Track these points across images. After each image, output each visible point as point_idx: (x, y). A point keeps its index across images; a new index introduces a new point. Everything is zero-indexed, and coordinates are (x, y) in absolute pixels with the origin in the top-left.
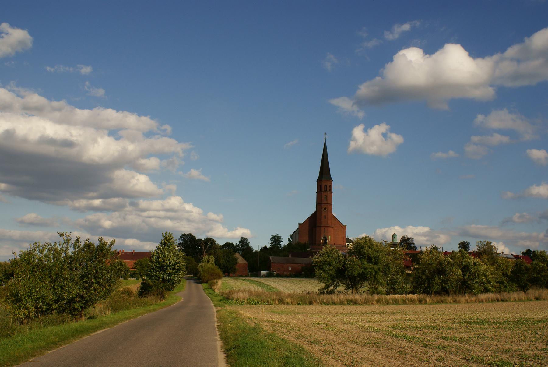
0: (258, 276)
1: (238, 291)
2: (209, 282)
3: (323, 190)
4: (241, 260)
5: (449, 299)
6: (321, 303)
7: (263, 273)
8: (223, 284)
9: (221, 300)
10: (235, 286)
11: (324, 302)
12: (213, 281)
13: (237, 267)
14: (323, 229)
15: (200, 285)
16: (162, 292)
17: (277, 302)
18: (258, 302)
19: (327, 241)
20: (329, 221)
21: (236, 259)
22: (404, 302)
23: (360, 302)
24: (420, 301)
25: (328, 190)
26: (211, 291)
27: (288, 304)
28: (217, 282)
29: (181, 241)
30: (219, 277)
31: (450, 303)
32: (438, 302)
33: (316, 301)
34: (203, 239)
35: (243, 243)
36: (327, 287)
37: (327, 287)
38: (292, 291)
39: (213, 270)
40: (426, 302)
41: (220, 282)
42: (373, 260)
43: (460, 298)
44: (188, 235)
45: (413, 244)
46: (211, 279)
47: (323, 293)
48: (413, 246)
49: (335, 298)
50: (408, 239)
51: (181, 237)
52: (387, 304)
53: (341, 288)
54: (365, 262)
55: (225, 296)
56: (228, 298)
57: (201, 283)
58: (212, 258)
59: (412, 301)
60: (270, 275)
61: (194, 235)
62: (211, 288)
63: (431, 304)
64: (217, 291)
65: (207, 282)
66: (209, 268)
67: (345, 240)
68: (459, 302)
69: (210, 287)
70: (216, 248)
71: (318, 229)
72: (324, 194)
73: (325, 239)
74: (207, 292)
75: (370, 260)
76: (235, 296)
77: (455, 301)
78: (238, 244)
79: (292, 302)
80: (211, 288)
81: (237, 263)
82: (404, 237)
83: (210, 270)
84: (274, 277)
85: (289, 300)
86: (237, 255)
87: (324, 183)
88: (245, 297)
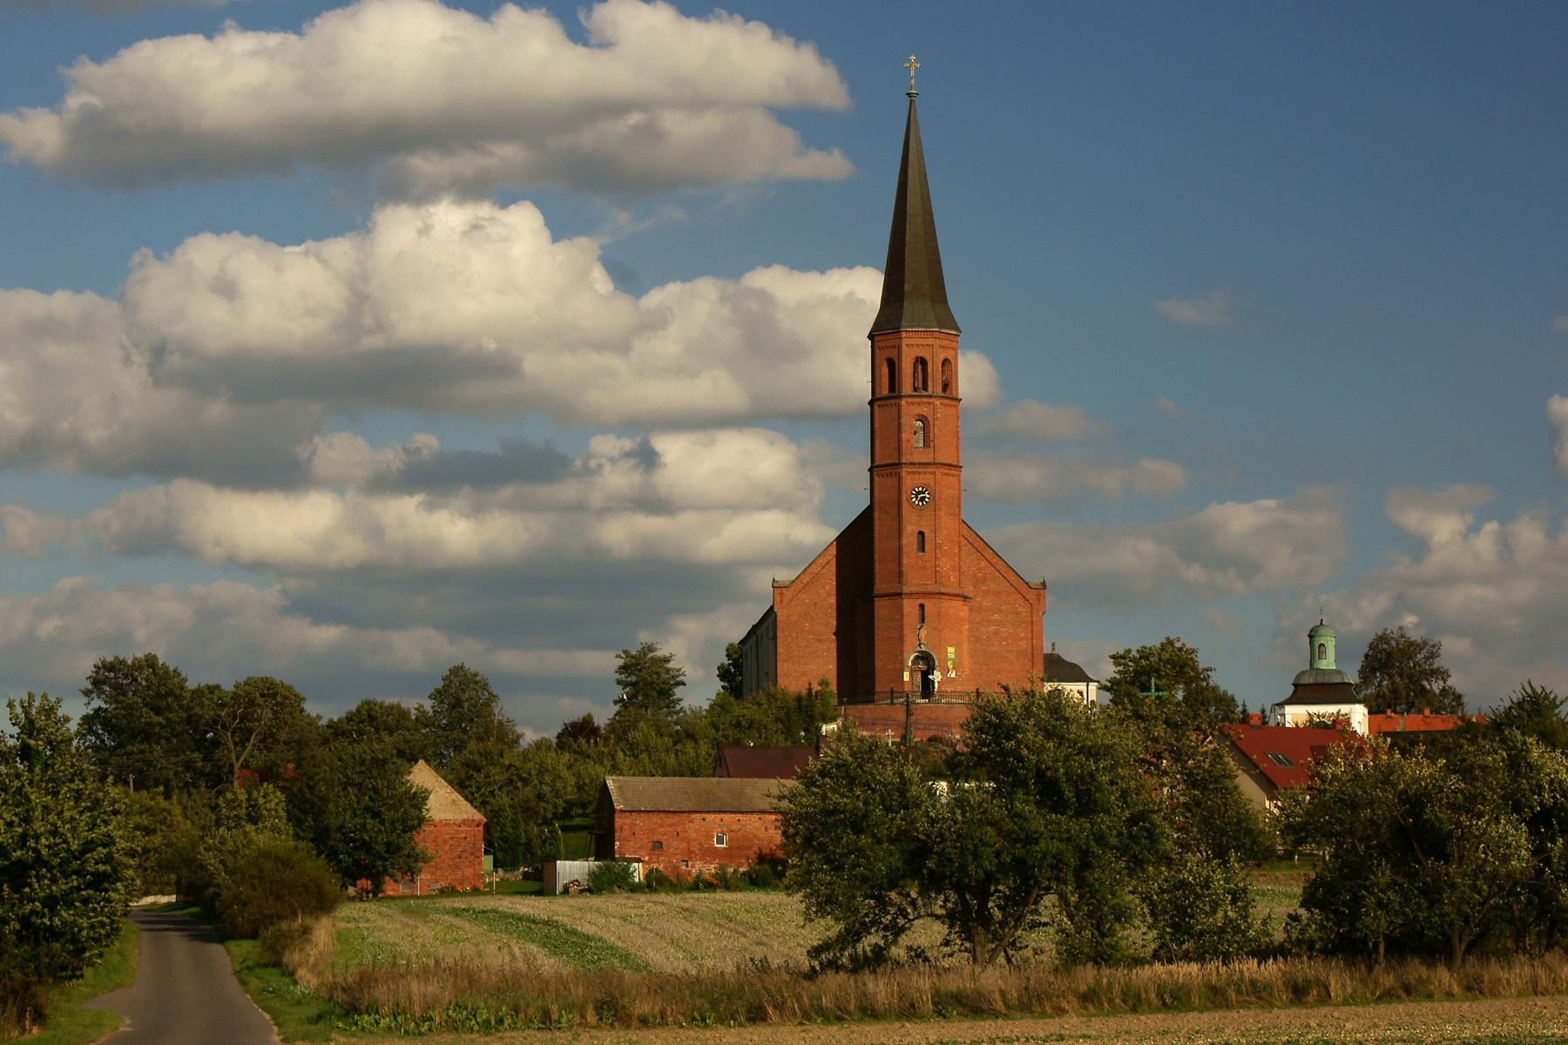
0: (541, 883)
1: (396, 973)
2: (268, 933)
3: (907, 386)
4: (444, 803)
5: (1443, 976)
6: (807, 1016)
7: (570, 869)
8: (341, 937)
9: (320, 1018)
10: (405, 947)
11: (821, 1011)
12: (284, 926)
13: (423, 841)
14: (910, 607)
15: (217, 950)
16: (27, 986)
17: (591, 1017)
18: (501, 1021)
19: (936, 676)
20: (945, 565)
21: (418, 799)
22: (1217, 997)
23: (1000, 1006)
24: (1298, 992)
25: (935, 386)
26: (274, 979)
27: (644, 1022)
28: (306, 931)
29: (98, 703)
30: (323, 904)
31: (1450, 995)
32: (1388, 996)
33: (779, 1007)
34: (228, 687)
35: (457, 703)
36: (853, 935)
37: (853, 935)
38: (709, 963)
39: (285, 862)
40: (1325, 999)
41: (323, 932)
42: (1069, 793)
43: (1494, 971)
44: (138, 666)
45: (1442, 674)
46: (280, 917)
47: (833, 965)
48: (1436, 686)
49: (879, 987)
50: (1409, 648)
51: (97, 683)
52: (1134, 1009)
53: (927, 932)
54: (1025, 805)
55: (340, 996)
56: (351, 1010)
57: (223, 937)
58: (273, 799)
59: (1259, 994)
60: (609, 881)
61: (163, 657)
62: (277, 964)
63: (1346, 1003)
64: (307, 980)
65: (253, 935)
66: (264, 854)
67: (1039, 670)
68: (1494, 994)
69: (268, 957)
70: (301, 744)
71: (882, 608)
72: (910, 410)
73: (927, 662)
74: (254, 983)
75: (1049, 793)
76: (381, 993)
77: (1474, 989)
78: (428, 705)
79: (663, 1014)
80: (277, 964)
81: (421, 820)
82: (1383, 638)
83: (268, 866)
84: (635, 889)
85: (643, 1008)
86: (422, 775)
87: (911, 346)
88: (436, 999)
